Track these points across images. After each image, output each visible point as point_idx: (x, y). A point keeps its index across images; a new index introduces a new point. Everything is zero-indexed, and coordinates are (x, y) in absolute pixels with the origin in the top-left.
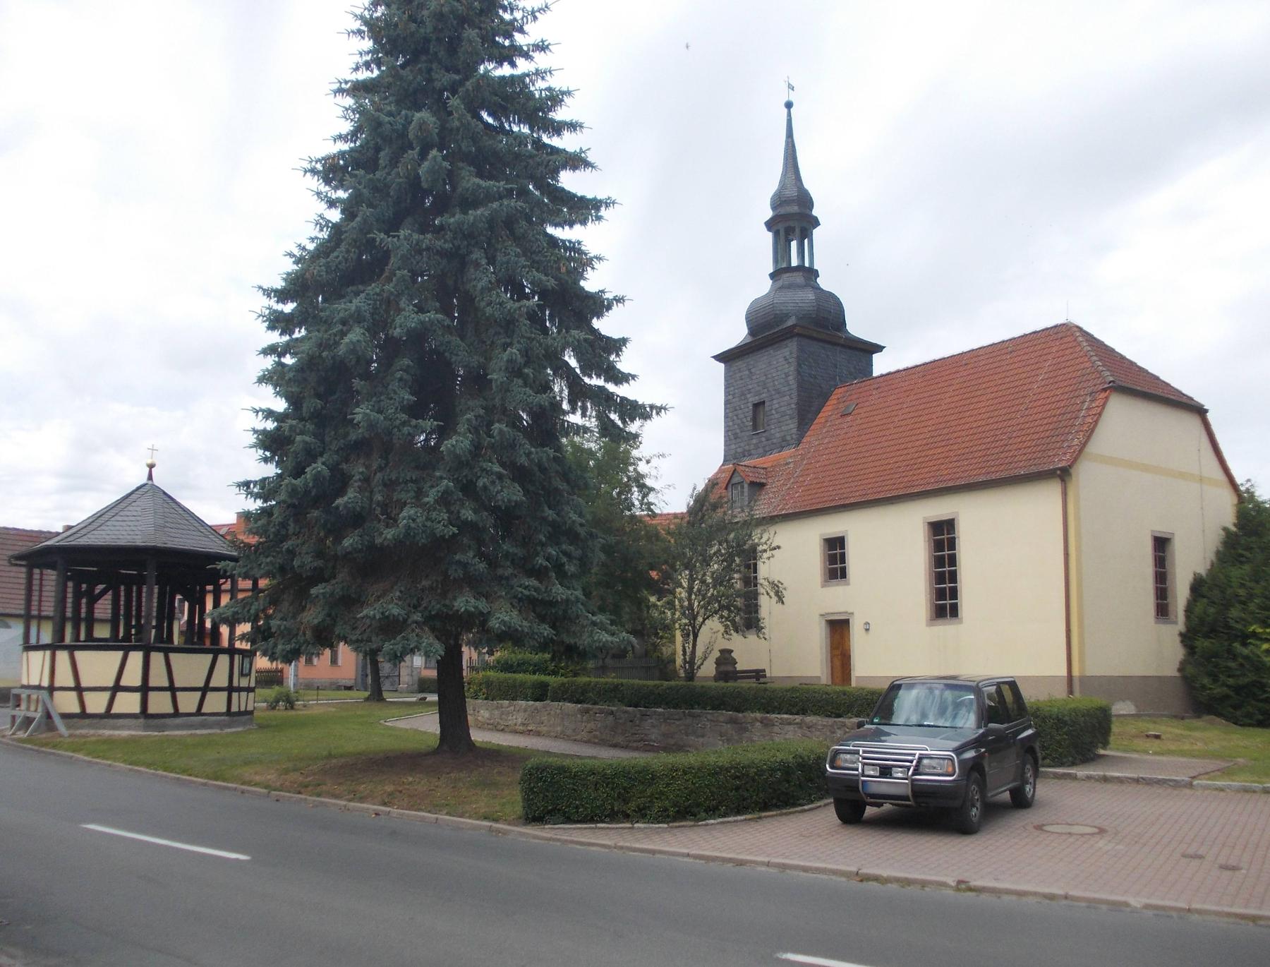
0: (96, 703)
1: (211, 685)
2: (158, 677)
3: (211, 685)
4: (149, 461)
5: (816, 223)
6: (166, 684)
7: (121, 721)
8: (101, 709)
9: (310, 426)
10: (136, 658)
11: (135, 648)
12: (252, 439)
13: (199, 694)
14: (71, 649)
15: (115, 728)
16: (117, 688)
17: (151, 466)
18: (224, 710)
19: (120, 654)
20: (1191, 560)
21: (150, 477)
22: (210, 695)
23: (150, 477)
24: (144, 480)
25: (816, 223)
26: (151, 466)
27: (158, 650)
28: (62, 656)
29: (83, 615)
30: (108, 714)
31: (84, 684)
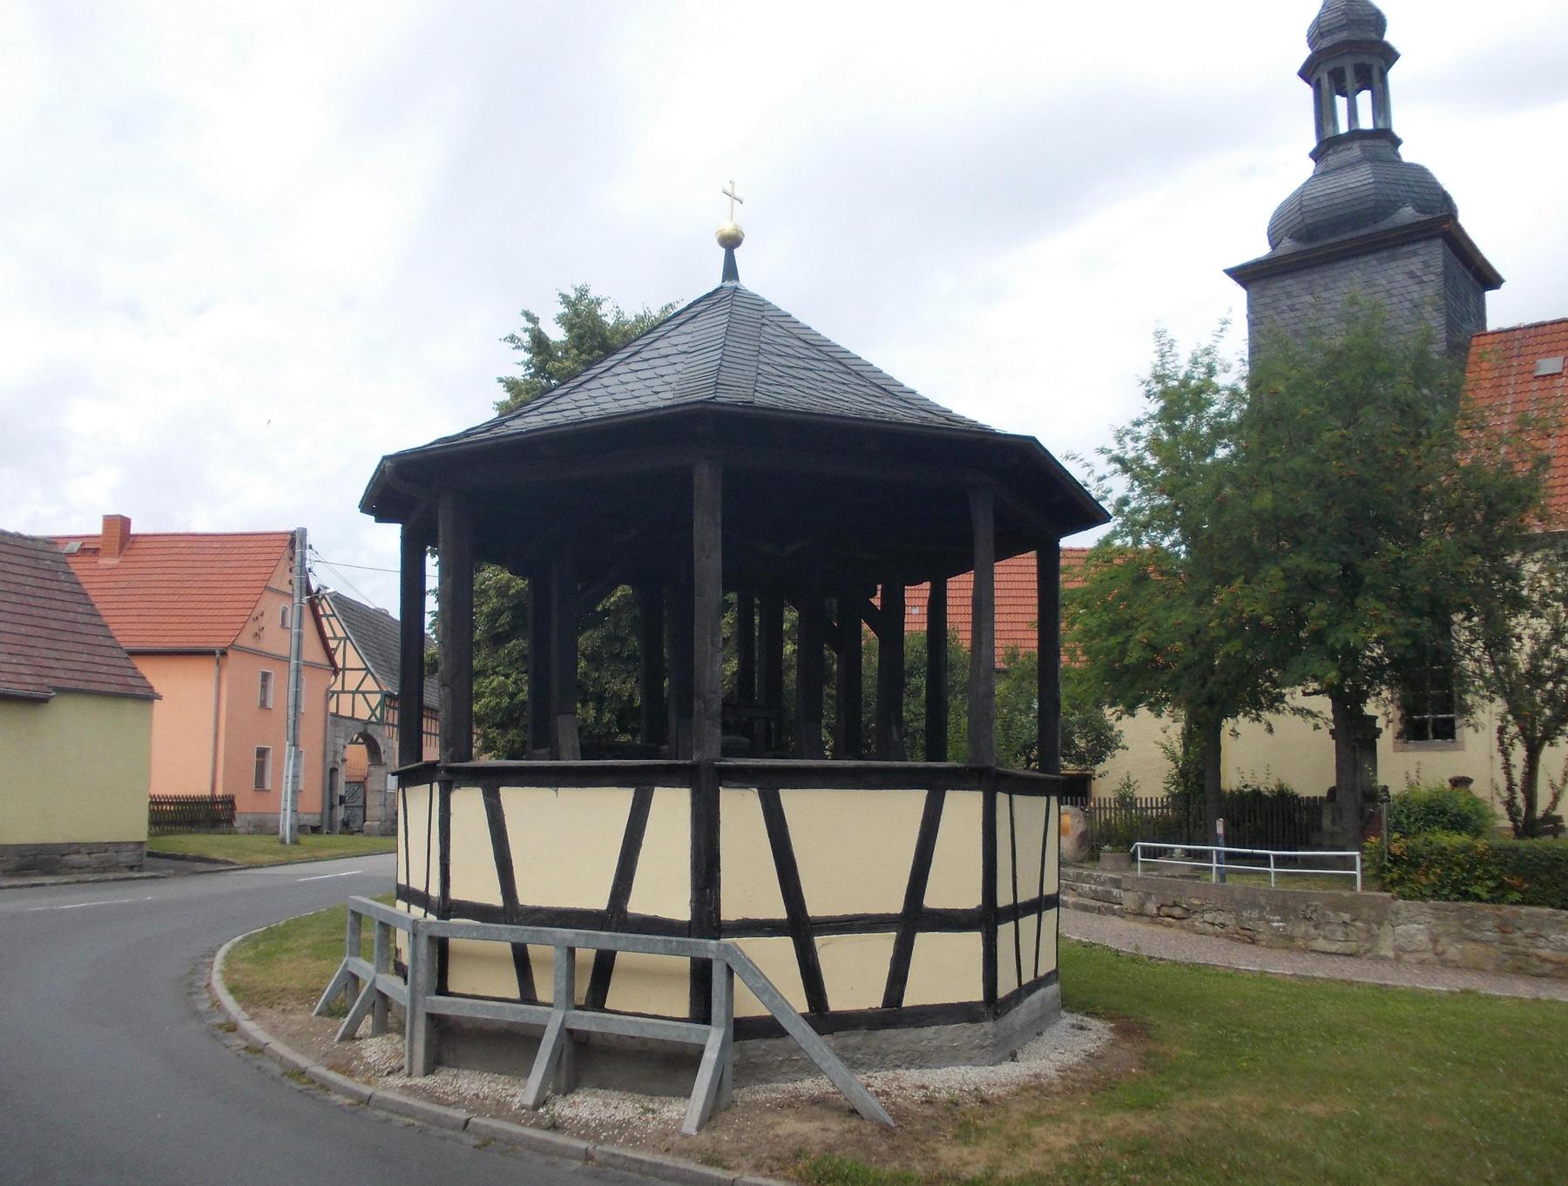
0: (855, 974)
1: (780, 912)
2: (749, 888)
3: (780, 912)
4: (728, 228)
5: (1390, 56)
6: (777, 910)
7: (928, 1035)
8: (871, 997)
9: (1552, 510)
10: (672, 808)
11: (671, 777)
12: (1181, 365)
13: (885, 943)
14: (491, 781)
15: (919, 1060)
16: (915, 918)
17: (730, 243)
18: (977, 995)
19: (623, 799)
20: (1246, 358)
21: (730, 271)
22: (925, 942)
23: (730, 271)
24: (714, 280)
25: (1390, 56)
26: (730, 243)
27: (741, 778)
28: (468, 803)
29: (830, 690)
30: (893, 1013)
31: (816, 908)
